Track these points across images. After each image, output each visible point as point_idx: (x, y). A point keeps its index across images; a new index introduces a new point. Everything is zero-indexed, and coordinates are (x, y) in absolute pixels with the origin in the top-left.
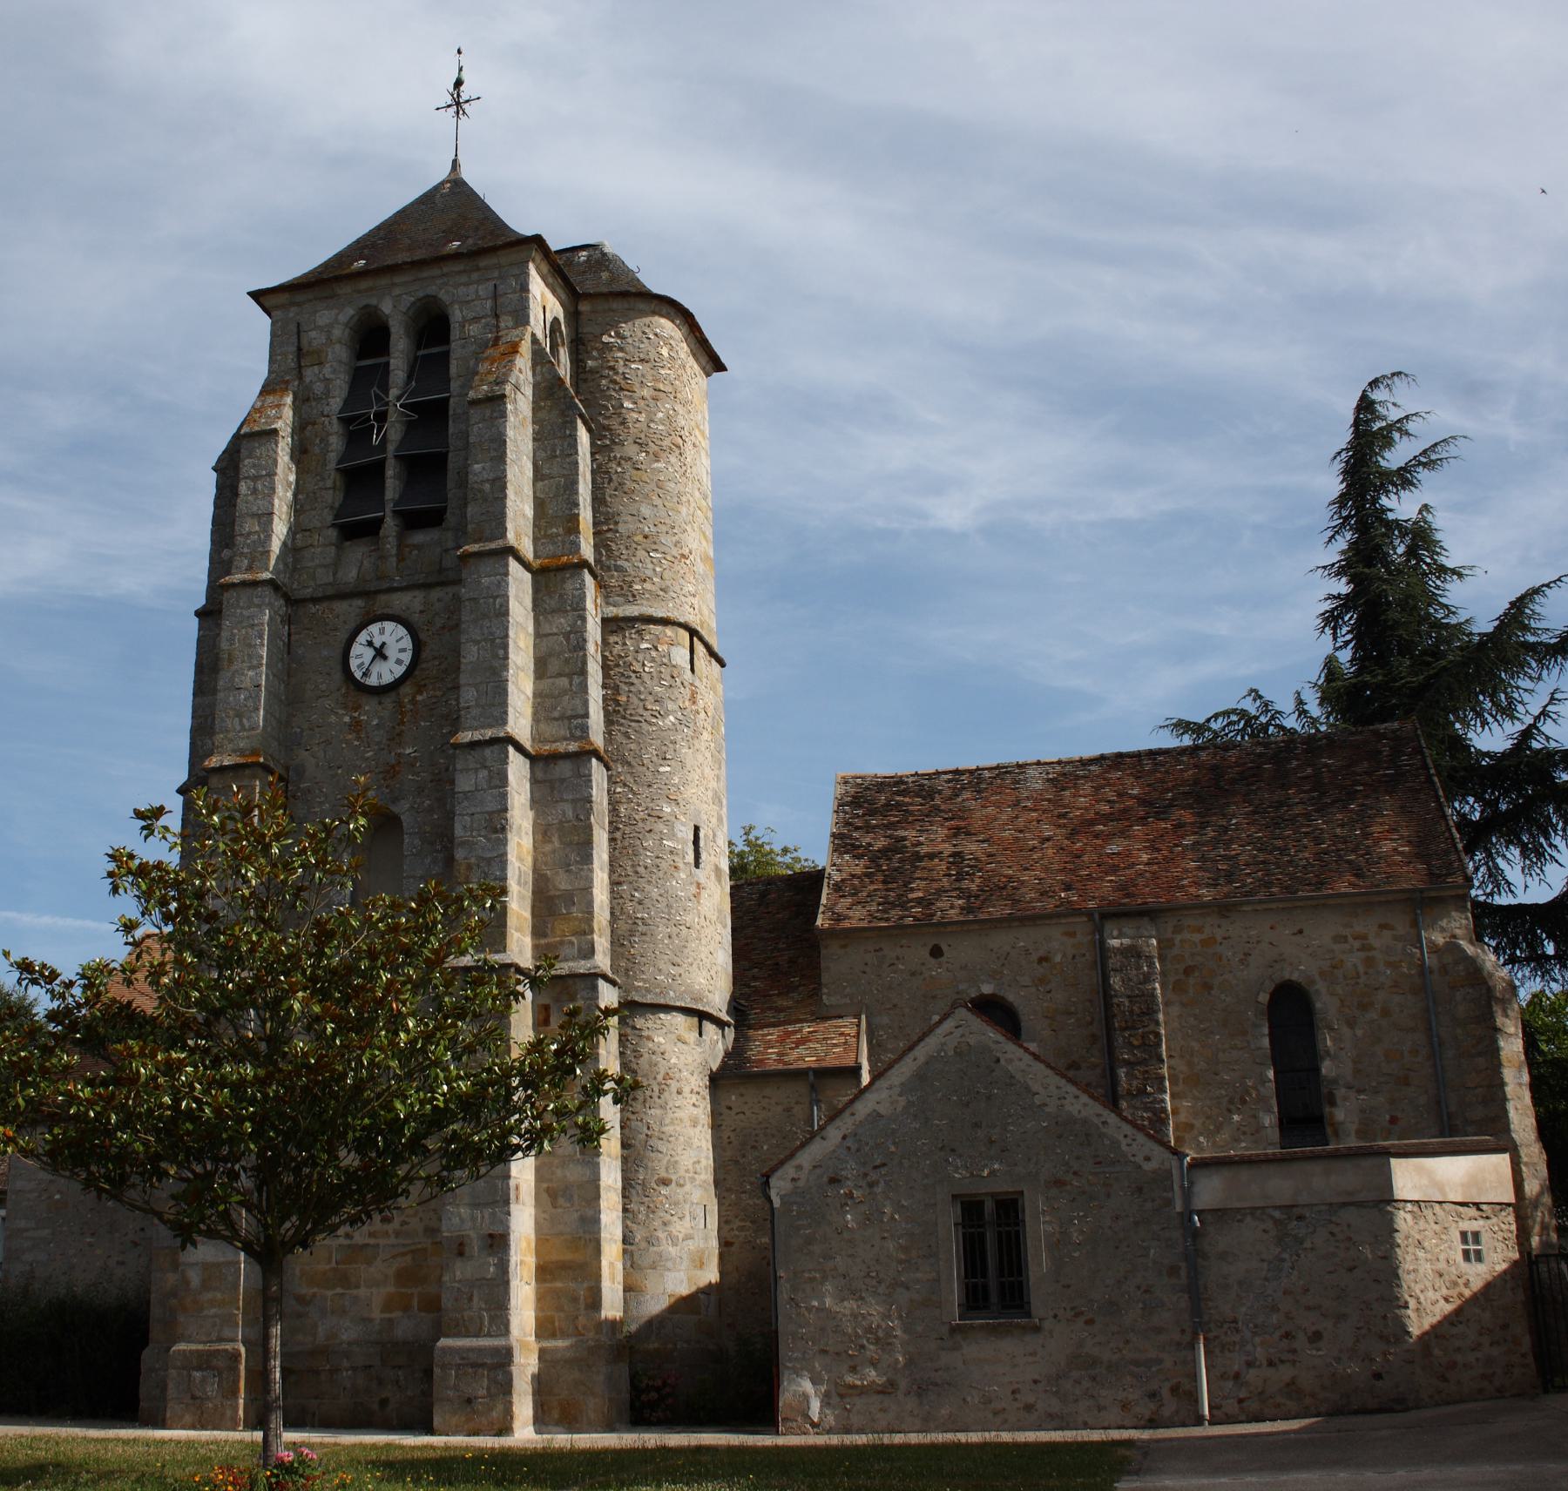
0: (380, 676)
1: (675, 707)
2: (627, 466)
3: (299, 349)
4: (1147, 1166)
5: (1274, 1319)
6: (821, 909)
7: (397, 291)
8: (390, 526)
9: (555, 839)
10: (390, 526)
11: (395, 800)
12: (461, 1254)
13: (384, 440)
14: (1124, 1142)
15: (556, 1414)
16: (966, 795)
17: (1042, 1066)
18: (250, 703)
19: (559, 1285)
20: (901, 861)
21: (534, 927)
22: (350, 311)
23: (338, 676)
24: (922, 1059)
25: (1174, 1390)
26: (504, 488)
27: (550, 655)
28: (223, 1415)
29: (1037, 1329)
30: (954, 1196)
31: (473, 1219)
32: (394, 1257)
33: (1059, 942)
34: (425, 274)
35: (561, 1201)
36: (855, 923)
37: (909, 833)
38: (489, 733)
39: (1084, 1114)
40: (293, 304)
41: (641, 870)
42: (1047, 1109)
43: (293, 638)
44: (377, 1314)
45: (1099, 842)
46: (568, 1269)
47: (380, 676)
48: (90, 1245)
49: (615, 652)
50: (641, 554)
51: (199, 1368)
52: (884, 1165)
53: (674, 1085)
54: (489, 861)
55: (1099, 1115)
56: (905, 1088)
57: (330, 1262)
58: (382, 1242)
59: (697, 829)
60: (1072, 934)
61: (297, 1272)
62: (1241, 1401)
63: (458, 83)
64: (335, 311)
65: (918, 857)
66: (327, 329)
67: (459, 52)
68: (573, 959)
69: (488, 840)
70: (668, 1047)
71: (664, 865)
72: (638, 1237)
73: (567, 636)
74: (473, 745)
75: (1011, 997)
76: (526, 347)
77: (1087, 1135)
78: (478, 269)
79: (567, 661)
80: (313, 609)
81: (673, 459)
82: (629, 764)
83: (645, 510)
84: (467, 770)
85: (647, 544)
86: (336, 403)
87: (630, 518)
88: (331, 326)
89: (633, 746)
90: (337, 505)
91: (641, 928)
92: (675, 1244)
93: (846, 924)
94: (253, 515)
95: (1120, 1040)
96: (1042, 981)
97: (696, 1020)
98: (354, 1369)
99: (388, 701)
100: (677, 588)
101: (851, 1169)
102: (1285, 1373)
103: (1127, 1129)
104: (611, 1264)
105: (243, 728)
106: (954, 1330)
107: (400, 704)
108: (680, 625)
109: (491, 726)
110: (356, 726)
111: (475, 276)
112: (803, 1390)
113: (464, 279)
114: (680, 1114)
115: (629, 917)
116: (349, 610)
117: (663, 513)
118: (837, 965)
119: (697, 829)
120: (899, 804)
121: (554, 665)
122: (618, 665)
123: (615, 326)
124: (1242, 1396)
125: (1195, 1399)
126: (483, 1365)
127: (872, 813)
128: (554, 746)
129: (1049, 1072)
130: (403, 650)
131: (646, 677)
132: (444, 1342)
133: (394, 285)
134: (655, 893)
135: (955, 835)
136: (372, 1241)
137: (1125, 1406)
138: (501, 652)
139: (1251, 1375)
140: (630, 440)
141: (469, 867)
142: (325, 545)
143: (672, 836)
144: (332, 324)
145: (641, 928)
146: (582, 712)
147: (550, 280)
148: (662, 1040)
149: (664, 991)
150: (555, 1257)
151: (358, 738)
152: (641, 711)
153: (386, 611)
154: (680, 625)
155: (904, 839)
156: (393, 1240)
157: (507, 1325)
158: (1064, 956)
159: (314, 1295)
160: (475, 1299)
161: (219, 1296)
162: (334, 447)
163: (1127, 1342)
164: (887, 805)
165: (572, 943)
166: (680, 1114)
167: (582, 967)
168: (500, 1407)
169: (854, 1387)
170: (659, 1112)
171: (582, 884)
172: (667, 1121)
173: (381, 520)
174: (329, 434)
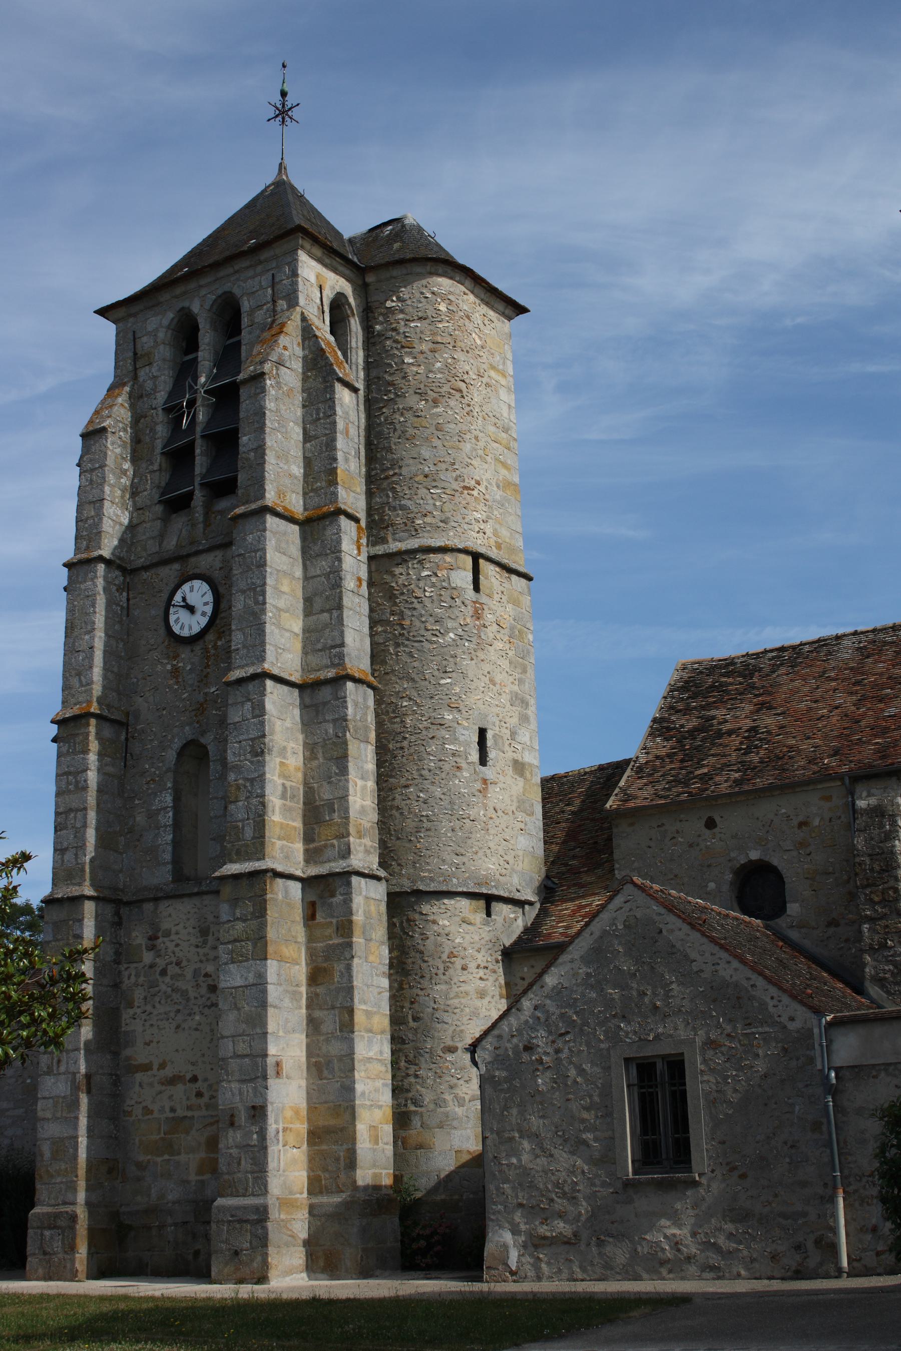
0: (190, 628)
1: (456, 625)
2: (408, 415)
3: (135, 354)
4: (792, 1026)
6: (617, 790)
7: (203, 292)
8: (199, 497)
9: (320, 755)
10: (199, 497)
11: (203, 733)
12: (232, 1124)
13: (193, 422)
14: (771, 1003)
15: (321, 1263)
16: (783, 670)
17: (698, 935)
18: (86, 663)
19: (324, 1147)
20: (704, 740)
21: (305, 833)
22: (171, 315)
23: (162, 631)
24: (597, 934)
25: (818, 1242)
26: (264, 454)
27: (315, 595)
28: (65, 1267)
30: (627, 1060)
31: (241, 1093)
32: (205, 1127)
33: (816, 807)
34: (222, 273)
35: (326, 1073)
36: (639, 803)
37: (719, 713)
38: (251, 670)
39: (735, 978)
40: (130, 315)
41: (424, 772)
42: (703, 975)
43: (131, 602)
45: (882, 705)
46: (331, 1135)
47: (190, 628)
49: (400, 582)
50: (422, 492)
51: (50, 1228)
52: (568, 1033)
53: (458, 963)
54: (252, 781)
55: (748, 979)
56: (586, 960)
57: (159, 1133)
58: (196, 1114)
59: (482, 733)
60: (828, 798)
61: (137, 1141)
62: (878, 1254)
63: (284, 94)
64: (159, 318)
65: (720, 734)
67: (284, 66)
68: (334, 860)
69: (252, 762)
70: (453, 929)
71: (446, 767)
72: (427, 1100)
73: (327, 576)
74: (240, 681)
75: (775, 862)
76: (293, 326)
77: (738, 998)
78: (261, 262)
79: (327, 598)
80: (145, 575)
81: (452, 403)
82: (413, 680)
83: (426, 453)
84: (236, 704)
85: (428, 482)
86: (161, 397)
87: (411, 461)
88: (157, 330)
89: (416, 664)
90: (163, 484)
91: (426, 824)
92: (461, 1105)
93: (631, 804)
94: (90, 503)
95: (862, 897)
96: (802, 844)
97: (482, 903)
98: (175, 1224)
99: (198, 648)
100: (459, 518)
101: (541, 1038)
103: (773, 991)
104: (373, 1128)
105: (82, 686)
106: (627, 1184)
107: (206, 650)
108: (460, 551)
109: (253, 664)
110: (175, 672)
111: (259, 269)
112: (505, 1241)
113: (250, 273)
114: (464, 988)
115: (416, 815)
116: (170, 572)
117: (442, 452)
118: (628, 842)
119: (482, 733)
120: (721, 685)
121: (318, 603)
122: (403, 594)
123: (395, 291)
124: (879, 1249)
125: (833, 1248)
126: (247, 1221)
127: (694, 697)
128: (318, 674)
129: (705, 940)
130: (206, 604)
131: (427, 602)
132: (220, 1201)
133: (201, 286)
134: (438, 792)
135: (758, 711)
136: (189, 1114)
137: (774, 1257)
138: (261, 598)
140: (411, 391)
141: (238, 788)
142: (154, 520)
143: (455, 740)
144: (158, 325)
145: (426, 824)
146: (338, 642)
147: (327, 261)
148: (446, 923)
149: (447, 879)
150: (321, 1123)
151: (177, 683)
152: (422, 632)
153: (197, 571)
154: (460, 551)
155: (713, 718)
156: (204, 1112)
157: (266, 1185)
158: (822, 819)
159: (149, 1161)
160: (243, 1162)
162: (159, 435)
163: (776, 1196)
164: (712, 686)
165: (333, 846)
166: (464, 988)
167: (338, 866)
168: (259, 1258)
169: (545, 1238)
170: (443, 987)
171: (340, 793)
172: (452, 995)
173: (190, 495)
174: (156, 424)
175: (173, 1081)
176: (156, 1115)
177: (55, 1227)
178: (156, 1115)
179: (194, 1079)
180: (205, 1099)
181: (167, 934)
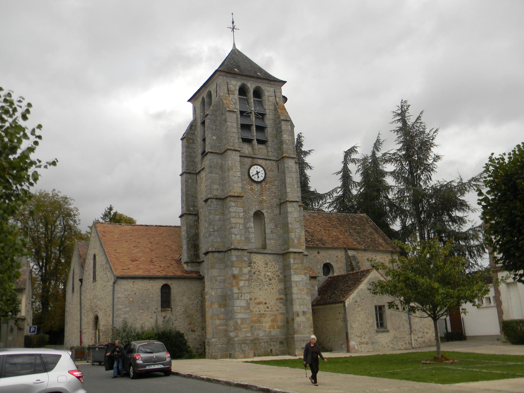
12: (298, 316)
23: (247, 176)
29: (388, 331)
44: (267, 330)
48: (142, 313)
51: (243, 344)
58: (267, 313)
63: (233, 23)
66: (235, 86)
99: (259, 185)
101: (358, 299)
102: (423, 339)
139: (418, 340)
156: (269, 312)
161: (245, 326)
175: (259, 303)
176: (254, 313)
177: (245, 343)
178: (254, 313)
179: (266, 303)
180: (270, 309)
181: (255, 263)
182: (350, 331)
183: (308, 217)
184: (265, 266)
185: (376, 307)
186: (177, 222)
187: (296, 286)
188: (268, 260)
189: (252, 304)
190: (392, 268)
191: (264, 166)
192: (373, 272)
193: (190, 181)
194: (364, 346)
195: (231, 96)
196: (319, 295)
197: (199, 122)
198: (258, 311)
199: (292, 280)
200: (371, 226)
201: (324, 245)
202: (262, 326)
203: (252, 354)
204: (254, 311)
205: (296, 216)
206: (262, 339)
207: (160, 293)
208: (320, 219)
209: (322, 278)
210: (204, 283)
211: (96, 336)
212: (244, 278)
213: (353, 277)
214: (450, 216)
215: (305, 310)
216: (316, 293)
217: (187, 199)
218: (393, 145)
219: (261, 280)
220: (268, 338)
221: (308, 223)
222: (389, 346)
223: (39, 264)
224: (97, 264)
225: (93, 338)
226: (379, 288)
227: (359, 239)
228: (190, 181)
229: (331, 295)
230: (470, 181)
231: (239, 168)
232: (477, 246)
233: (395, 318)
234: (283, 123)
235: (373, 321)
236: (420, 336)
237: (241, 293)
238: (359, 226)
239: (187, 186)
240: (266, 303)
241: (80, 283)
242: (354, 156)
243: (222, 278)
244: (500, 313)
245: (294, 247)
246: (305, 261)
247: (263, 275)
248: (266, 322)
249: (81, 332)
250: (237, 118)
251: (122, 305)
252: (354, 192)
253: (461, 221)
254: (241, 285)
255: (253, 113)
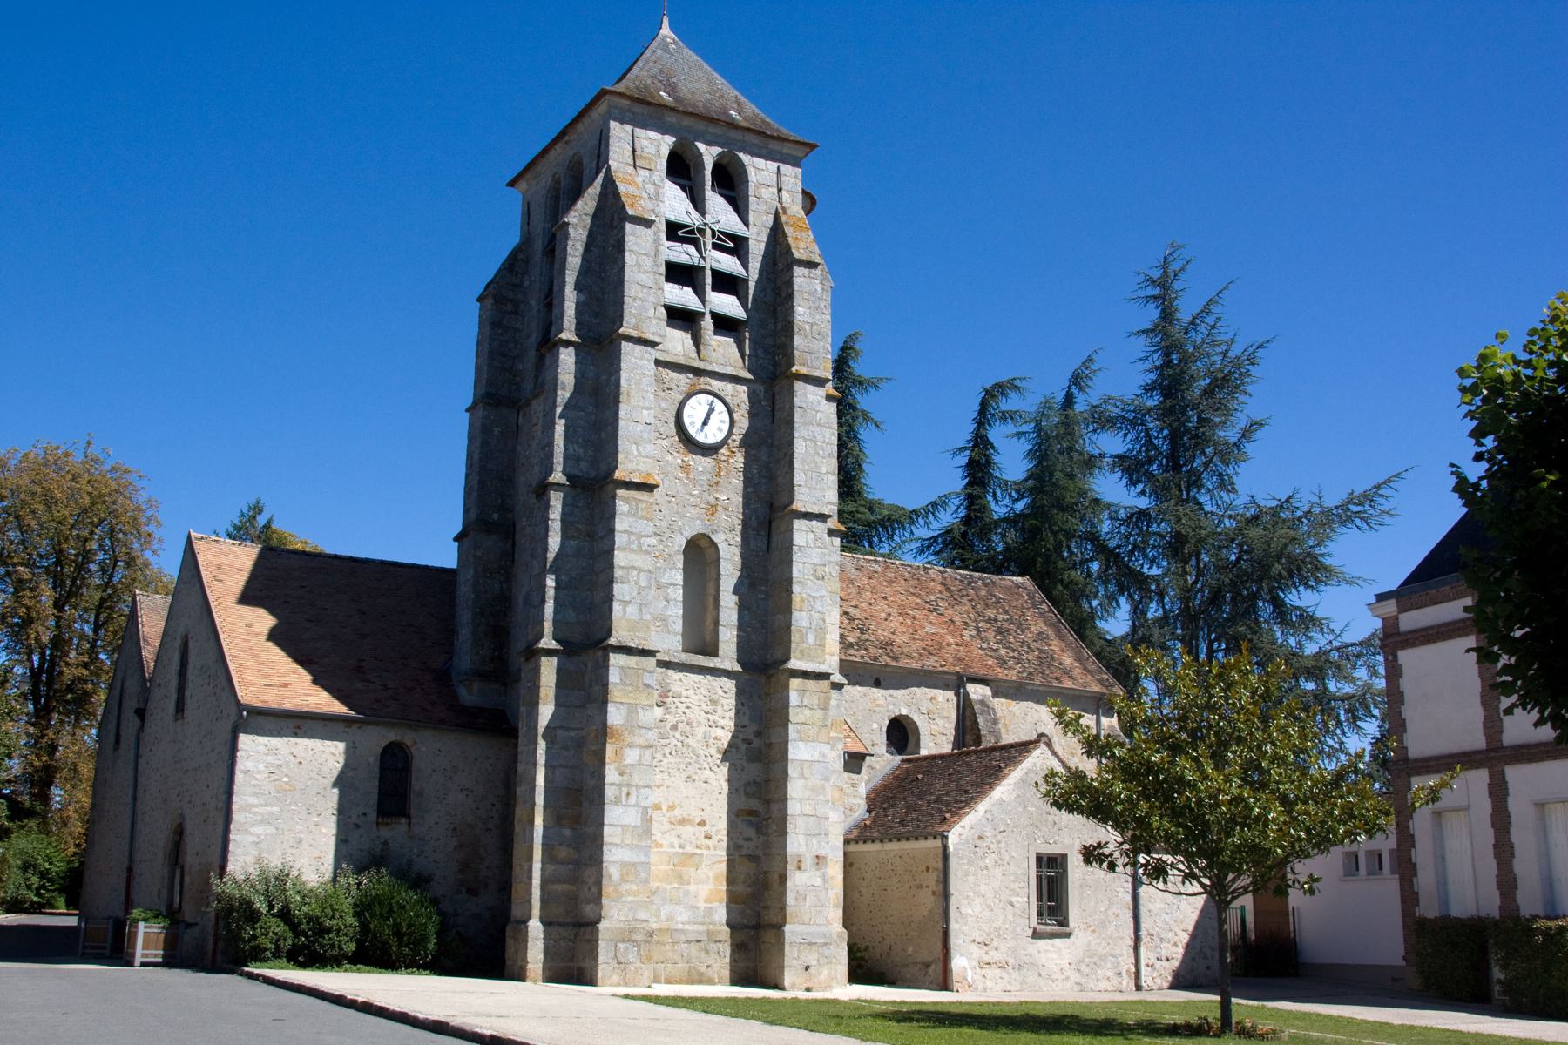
5: (1171, 935)
44: (702, 904)
48: (317, 824)
58: (705, 852)
101: (989, 833)
141: (803, 600)
161: (634, 887)
179: (702, 823)
182: (954, 926)
183: (852, 573)
184: (710, 708)
185: (1039, 858)
186: (446, 556)
187: (802, 776)
188: (720, 691)
189: (661, 822)
190: (1059, 768)
191: (728, 399)
192: (1037, 752)
193: (496, 431)
194: (992, 972)
195: (641, 172)
196: (869, 811)
197: (539, 245)
198: (676, 842)
199: (791, 756)
200: (1042, 615)
201: (895, 659)
202: (687, 893)
203: (647, 974)
204: (665, 843)
205: (817, 561)
206: (683, 931)
207: (377, 769)
208: (891, 582)
209: (884, 762)
210: (516, 746)
211: (171, 891)
212: (641, 741)
213: (978, 760)
214: (1278, 604)
215: (822, 853)
216: (860, 806)
217: (482, 483)
218: (1125, 376)
219: (694, 752)
220: (701, 928)
221: (853, 590)
222: (1068, 978)
223: (30, 660)
224: (190, 666)
225: (165, 892)
226: (1074, 795)
227: (1003, 652)
228: (496, 431)
229: (907, 814)
230: (1344, 506)
231: (652, 397)
232: (1350, 697)
233: (1096, 894)
234: (798, 271)
235: (1025, 897)
236: (1164, 953)
237: (628, 785)
238: (1006, 612)
239: (485, 443)
240: (702, 823)
241: (138, 722)
242: (1006, 405)
243: (572, 734)
244: (1409, 898)
245: (803, 655)
246: (833, 703)
247: (700, 736)
248: (698, 882)
249: (130, 870)
250: (657, 243)
251: (256, 794)
252: (999, 508)
253: (1308, 621)
254: (628, 761)
255: (709, 232)
